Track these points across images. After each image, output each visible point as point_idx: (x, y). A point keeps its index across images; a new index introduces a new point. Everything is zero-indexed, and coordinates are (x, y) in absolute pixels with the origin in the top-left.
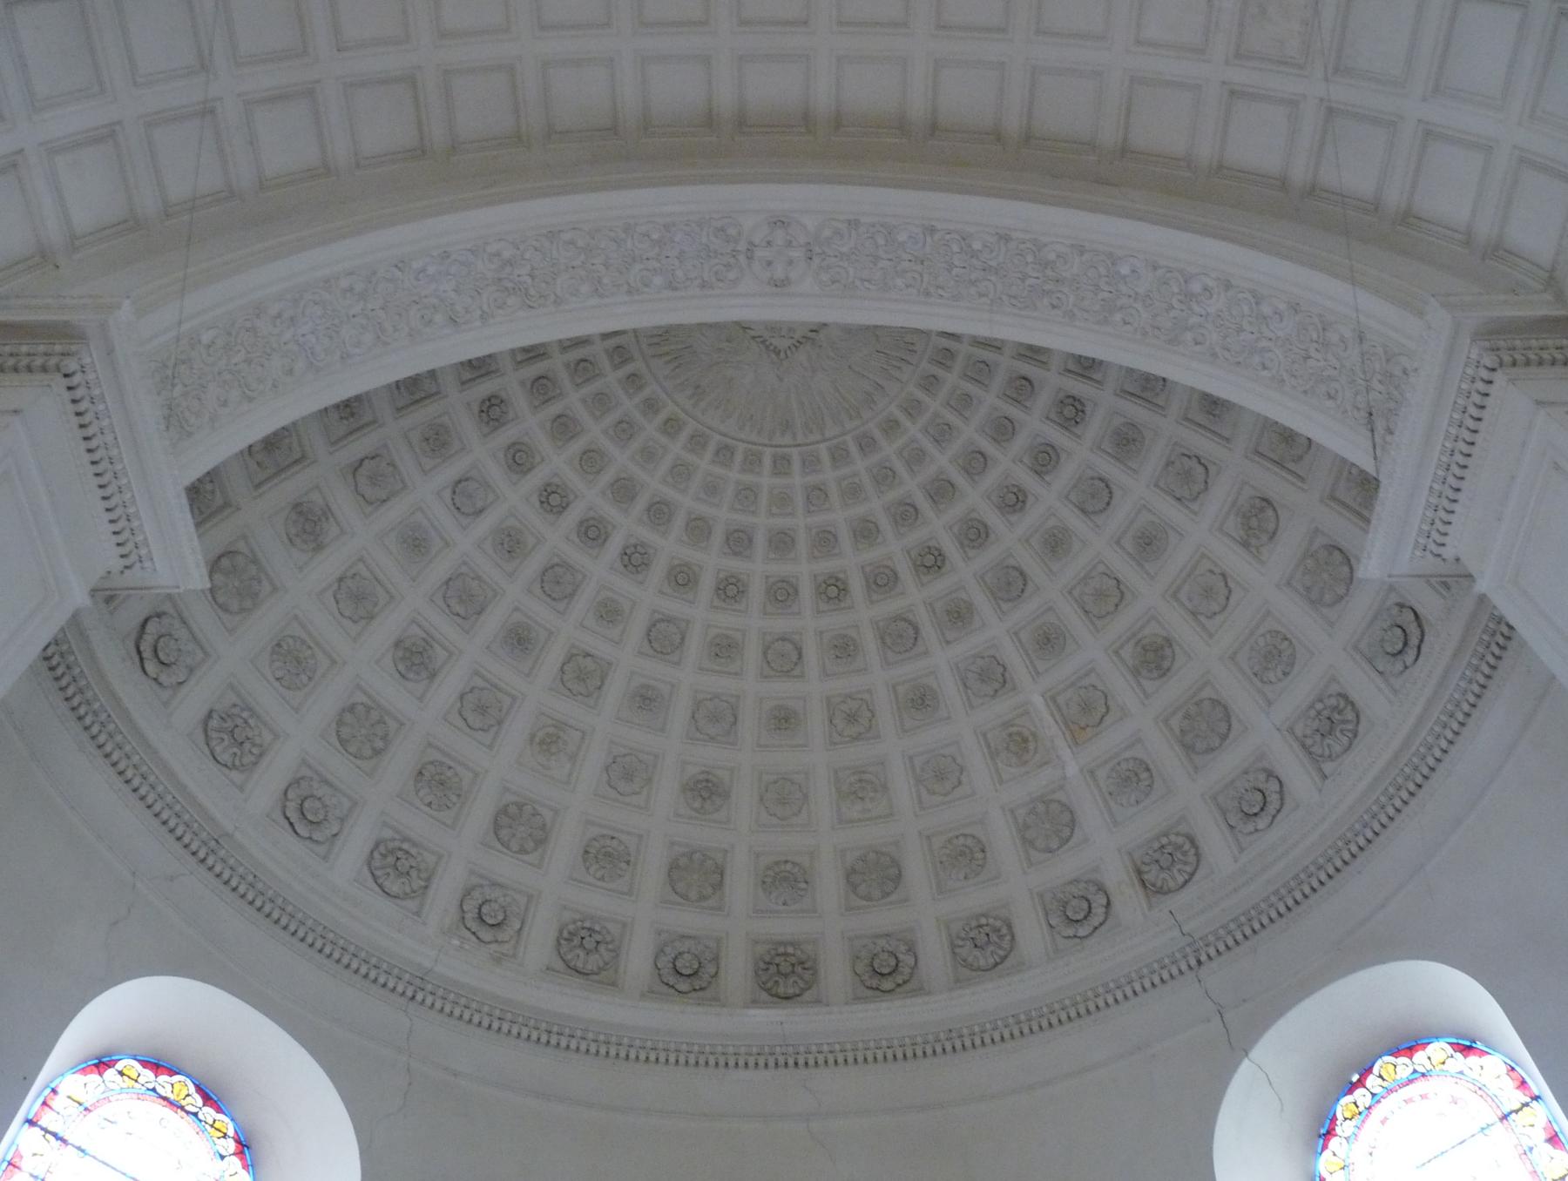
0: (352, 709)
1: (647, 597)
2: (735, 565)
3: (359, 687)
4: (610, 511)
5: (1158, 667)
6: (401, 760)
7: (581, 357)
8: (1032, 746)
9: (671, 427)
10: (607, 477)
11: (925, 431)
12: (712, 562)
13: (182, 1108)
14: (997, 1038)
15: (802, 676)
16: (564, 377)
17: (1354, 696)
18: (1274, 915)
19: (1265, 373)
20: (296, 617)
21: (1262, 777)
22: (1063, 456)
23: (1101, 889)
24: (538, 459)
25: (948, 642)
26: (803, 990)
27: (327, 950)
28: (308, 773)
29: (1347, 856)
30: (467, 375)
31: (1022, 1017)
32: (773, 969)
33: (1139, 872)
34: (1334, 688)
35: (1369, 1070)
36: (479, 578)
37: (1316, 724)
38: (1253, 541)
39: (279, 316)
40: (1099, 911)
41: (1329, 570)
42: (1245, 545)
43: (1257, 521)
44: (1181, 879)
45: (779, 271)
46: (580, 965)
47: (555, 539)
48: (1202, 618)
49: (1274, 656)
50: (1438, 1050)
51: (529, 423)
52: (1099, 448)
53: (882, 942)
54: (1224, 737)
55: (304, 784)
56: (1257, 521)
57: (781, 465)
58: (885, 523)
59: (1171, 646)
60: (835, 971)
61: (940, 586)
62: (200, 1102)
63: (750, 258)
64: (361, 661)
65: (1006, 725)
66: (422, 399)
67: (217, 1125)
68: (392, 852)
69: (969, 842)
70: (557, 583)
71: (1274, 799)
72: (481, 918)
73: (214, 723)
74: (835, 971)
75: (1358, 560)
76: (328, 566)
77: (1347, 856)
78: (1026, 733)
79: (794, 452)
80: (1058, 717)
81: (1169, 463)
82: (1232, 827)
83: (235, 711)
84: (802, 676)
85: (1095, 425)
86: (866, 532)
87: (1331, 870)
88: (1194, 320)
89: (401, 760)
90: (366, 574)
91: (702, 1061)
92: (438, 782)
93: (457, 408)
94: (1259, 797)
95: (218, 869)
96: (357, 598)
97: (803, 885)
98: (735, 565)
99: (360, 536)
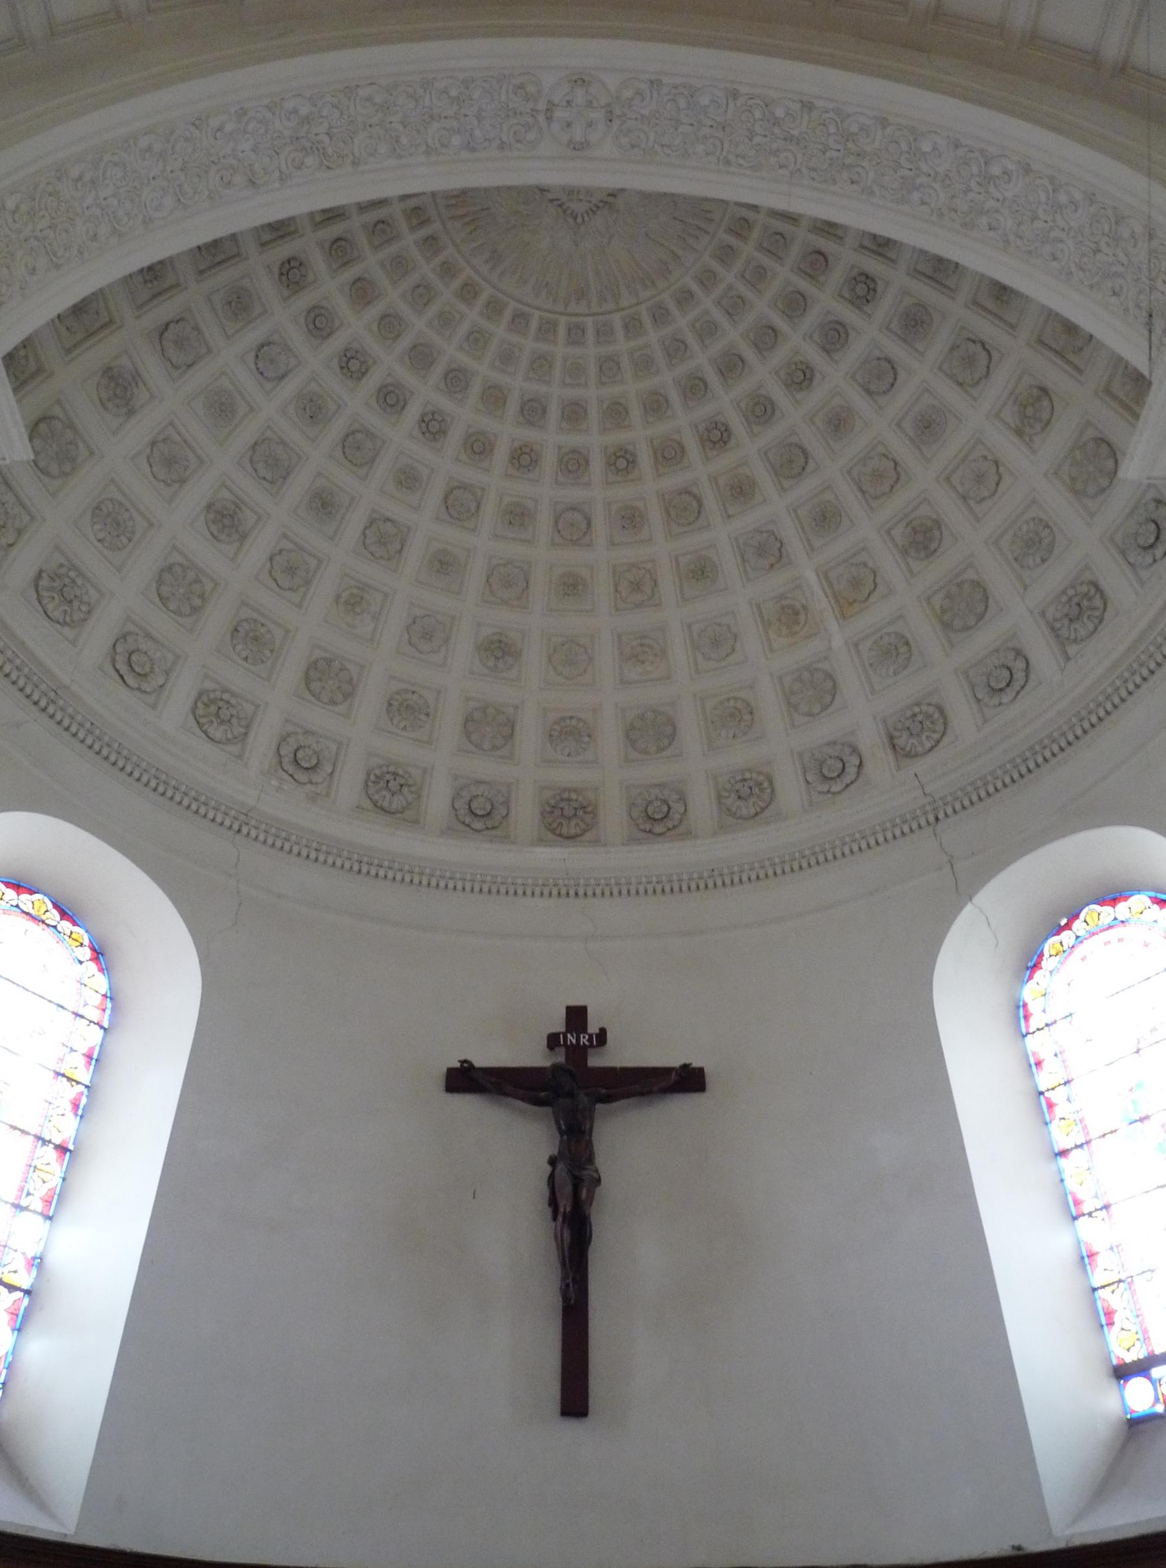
0: (170, 568)
1: (444, 464)
2: (529, 435)
3: (174, 548)
4: (408, 378)
5: (926, 548)
6: (217, 618)
7: (379, 220)
8: (802, 618)
9: (468, 292)
10: (405, 343)
11: (718, 303)
12: (507, 431)
13: (43, 922)
14: (753, 877)
15: (590, 545)
16: (362, 240)
17: (1104, 585)
18: (1008, 780)
19: (1055, 264)
20: (113, 481)
21: (1011, 655)
22: (852, 334)
23: (855, 750)
24: (337, 322)
25: (729, 516)
26: (585, 831)
27: (161, 789)
28: (132, 628)
29: (1079, 732)
30: (266, 237)
31: (777, 860)
32: (557, 812)
34: (1087, 576)
35: (1077, 916)
36: (282, 442)
37: (1066, 609)
38: (1027, 430)
39: (80, 178)
40: (851, 771)
41: (1097, 459)
42: (1019, 433)
43: (1032, 410)
44: (928, 745)
45: (578, 133)
46: (386, 804)
47: (355, 404)
48: (971, 503)
49: (1035, 542)
50: (1140, 901)
51: (328, 286)
52: (888, 328)
54: (981, 617)
55: (130, 639)
56: (1032, 410)
57: (576, 335)
58: (674, 396)
59: (939, 528)
60: (613, 815)
61: (725, 461)
62: (57, 916)
63: (549, 119)
64: (175, 523)
65: (782, 597)
66: (223, 261)
67: (74, 936)
68: (213, 701)
69: (739, 705)
70: (357, 448)
71: (1019, 676)
72: (296, 761)
73: (44, 582)
74: (613, 815)
75: (1124, 454)
76: (140, 431)
77: (1079, 732)
78: (798, 606)
79: (589, 321)
80: (828, 591)
81: (954, 347)
82: (978, 700)
83: (63, 571)
84: (590, 545)
85: (886, 305)
86: (656, 405)
87: (1063, 744)
88: (991, 204)
89: (217, 618)
90: (177, 438)
91: (494, 890)
92: (252, 639)
93: (258, 275)
94: (1006, 674)
95: (58, 716)
96: (170, 461)
97: (586, 739)
98: (529, 435)
99: (169, 401)
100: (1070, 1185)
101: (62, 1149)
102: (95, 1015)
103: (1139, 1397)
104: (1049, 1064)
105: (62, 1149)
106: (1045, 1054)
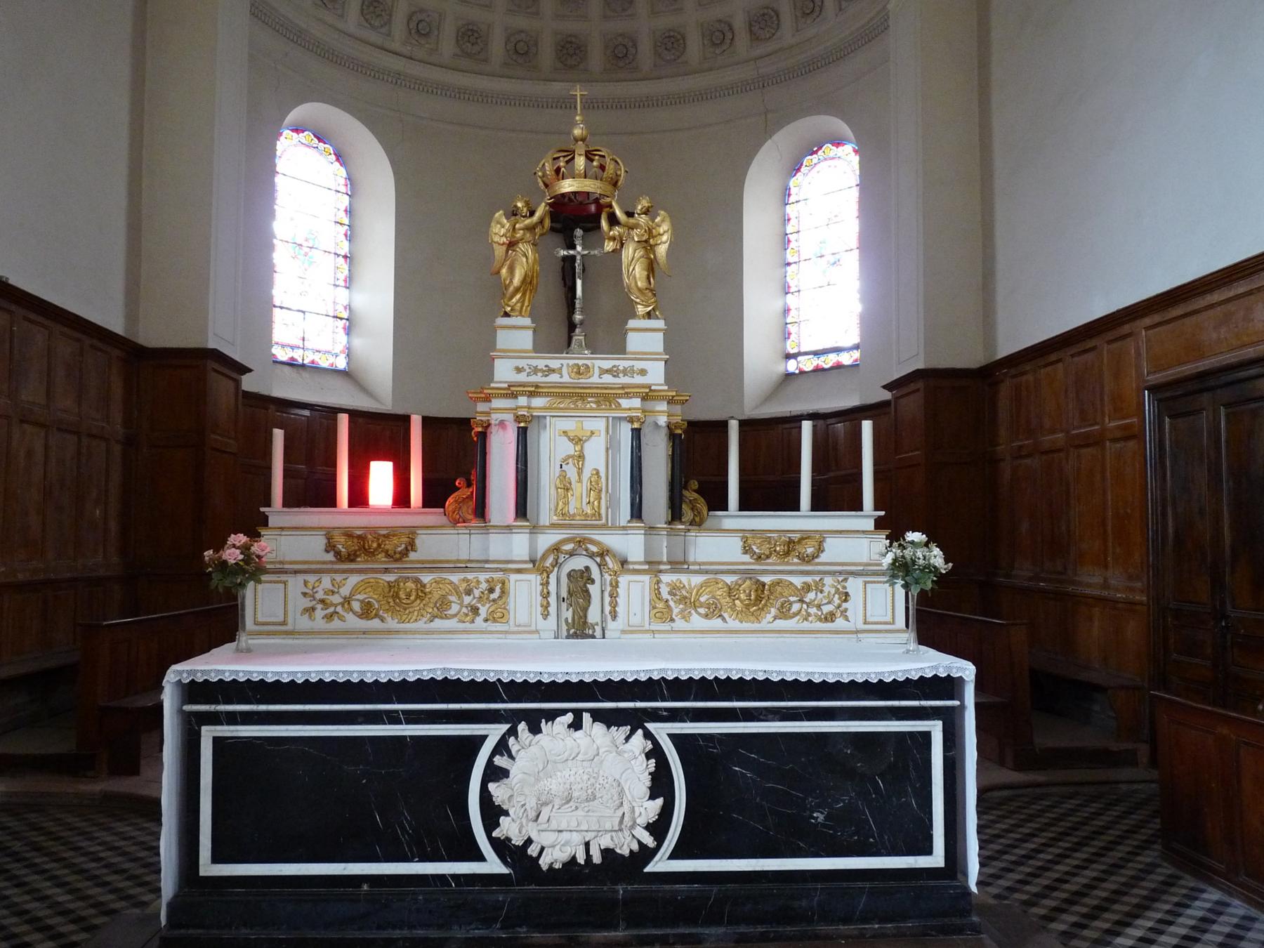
33: (750, 25)
53: (620, 39)
100: (788, 279)
101: (345, 257)
102: (343, 189)
103: (792, 366)
105: (345, 257)
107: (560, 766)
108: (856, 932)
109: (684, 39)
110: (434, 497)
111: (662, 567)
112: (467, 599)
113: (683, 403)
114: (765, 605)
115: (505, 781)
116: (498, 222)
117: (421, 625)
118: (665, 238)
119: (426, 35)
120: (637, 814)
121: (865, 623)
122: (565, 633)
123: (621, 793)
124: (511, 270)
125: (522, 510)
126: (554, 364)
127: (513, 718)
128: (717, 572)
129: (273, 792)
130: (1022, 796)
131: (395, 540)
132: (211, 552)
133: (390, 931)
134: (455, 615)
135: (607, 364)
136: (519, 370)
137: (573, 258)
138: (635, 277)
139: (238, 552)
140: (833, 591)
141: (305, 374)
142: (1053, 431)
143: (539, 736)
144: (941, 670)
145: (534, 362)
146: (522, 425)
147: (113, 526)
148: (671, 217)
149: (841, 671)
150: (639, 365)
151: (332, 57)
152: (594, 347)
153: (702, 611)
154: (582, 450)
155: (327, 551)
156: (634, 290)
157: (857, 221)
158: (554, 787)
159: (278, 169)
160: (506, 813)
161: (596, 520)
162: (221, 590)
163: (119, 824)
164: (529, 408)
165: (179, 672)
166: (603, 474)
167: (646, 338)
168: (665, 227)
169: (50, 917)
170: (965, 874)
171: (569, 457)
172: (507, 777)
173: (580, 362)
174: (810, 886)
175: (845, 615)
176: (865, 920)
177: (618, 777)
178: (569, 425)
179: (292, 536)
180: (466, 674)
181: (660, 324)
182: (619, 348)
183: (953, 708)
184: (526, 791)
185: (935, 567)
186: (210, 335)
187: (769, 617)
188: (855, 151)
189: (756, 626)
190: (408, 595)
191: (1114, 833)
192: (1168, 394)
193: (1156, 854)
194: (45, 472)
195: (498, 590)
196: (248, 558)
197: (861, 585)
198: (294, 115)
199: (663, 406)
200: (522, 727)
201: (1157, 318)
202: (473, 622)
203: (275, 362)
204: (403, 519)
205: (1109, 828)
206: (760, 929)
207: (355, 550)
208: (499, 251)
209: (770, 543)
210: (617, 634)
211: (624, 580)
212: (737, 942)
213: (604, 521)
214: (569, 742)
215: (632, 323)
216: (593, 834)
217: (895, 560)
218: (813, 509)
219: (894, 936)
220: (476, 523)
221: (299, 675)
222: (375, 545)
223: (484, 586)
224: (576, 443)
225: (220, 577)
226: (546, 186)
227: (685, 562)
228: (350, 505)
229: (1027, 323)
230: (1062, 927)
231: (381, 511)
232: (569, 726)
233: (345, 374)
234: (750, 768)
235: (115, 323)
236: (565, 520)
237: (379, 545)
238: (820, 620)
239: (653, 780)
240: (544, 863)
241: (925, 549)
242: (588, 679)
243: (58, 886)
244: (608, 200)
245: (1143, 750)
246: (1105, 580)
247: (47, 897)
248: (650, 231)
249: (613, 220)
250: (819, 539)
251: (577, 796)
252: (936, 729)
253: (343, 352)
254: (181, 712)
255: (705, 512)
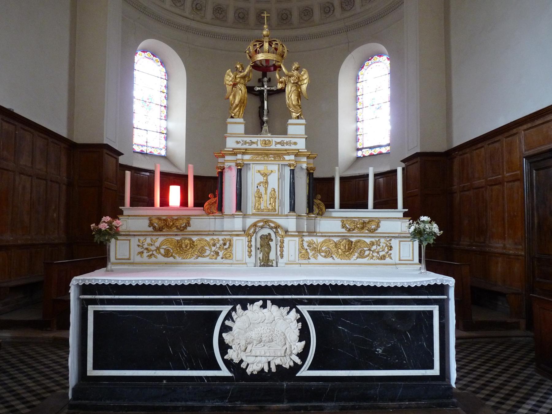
33: (341, 4)
53: (284, 11)
100: (358, 115)
101: (165, 107)
102: (164, 77)
103: (360, 154)
104: (360, 90)
105: (165, 107)
106: (360, 88)
107: (256, 326)
108: (397, 406)
109: (312, 11)
110: (198, 203)
111: (304, 234)
112: (214, 248)
113: (314, 158)
114: (353, 252)
115: (230, 332)
116: (228, 75)
117: (192, 260)
118: (305, 81)
119: (201, 10)
120: (293, 348)
121: (400, 260)
122: (259, 264)
123: (285, 339)
124: (234, 96)
125: (239, 207)
126: (254, 140)
127: (234, 302)
128: (330, 236)
129: (119, 337)
130: (467, 342)
131: (181, 222)
132: (94, 225)
133: (176, 403)
134: (208, 256)
135: (279, 140)
136: (238, 143)
137: (263, 91)
138: (291, 100)
139: (106, 224)
140: (385, 245)
141: (148, 157)
142: (479, 178)
143: (246, 311)
144: (438, 281)
145: (245, 139)
146: (239, 167)
147: (62, 221)
148: (309, 74)
149: (390, 281)
150: (293, 140)
151: (159, 19)
152: (273, 132)
153: (323, 254)
154: (267, 179)
155: (149, 226)
156: (291, 106)
157: (389, 89)
158: (253, 335)
159: (135, 68)
160: (231, 348)
161: (273, 212)
162: (99, 242)
163: (59, 351)
164: (242, 160)
165: (77, 281)
166: (277, 190)
167: (297, 128)
168: (306, 76)
169: (24, 393)
170: (449, 379)
171: (261, 182)
172: (231, 330)
173: (266, 139)
174: (375, 383)
175: (391, 257)
176: (401, 400)
177: (284, 331)
178: (261, 168)
179: (133, 219)
180: (212, 281)
181: (303, 121)
182: (284, 132)
183: (444, 299)
184: (240, 337)
185: (435, 233)
186: (105, 138)
187: (355, 257)
188: (388, 59)
189: (348, 261)
190: (186, 246)
191: (512, 360)
192: (535, 159)
193: (533, 369)
194: (31, 197)
195: (228, 244)
196: (111, 228)
197: (398, 242)
198: (143, 44)
199: (305, 159)
200: (238, 307)
201: (529, 125)
202: (216, 259)
203: (135, 152)
204: (184, 212)
205: (509, 358)
206: (351, 404)
207: (162, 226)
208: (229, 88)
209: (354, 223)
210: (283, 265)
211: (286, 240)
212: (341, 409)
213: (277, 212)
214: (261, 314)
215: (290, 121)
216: (272, 358)
217: (415, 230)
218: (374, 208)
219: (416, 408)
220: (218, 214)
221: (134, 282)
222: (171, 223)
223: (221, 242)
224: (264, 176)
225: (99, 236)
226: (250, 57)
227: (315, 232)
228: (161, 206)
229: (466, 131)
230: (493, 404)
231: (174, 209)
232: (261, 307)
233: (164, 157)
234: (346, 327)
235: (63, 132)
236: (259, 212)
237: (173, 224)
238: (379, 259)
239: (300, 332)
240: (249, 371)
241: (429, 224)
242: (269, 284)
243: (30, 379)
244: (279, 63)
245: (523, 323)
246: (504, 245)
247: (24, 384)
248: (299, 78)
249: (282, 74)
250: (378, 222)
251: (264, 339)
252: (435, 309)
253: (164, 148)
254: (79, 299)
255: (324, 210)
